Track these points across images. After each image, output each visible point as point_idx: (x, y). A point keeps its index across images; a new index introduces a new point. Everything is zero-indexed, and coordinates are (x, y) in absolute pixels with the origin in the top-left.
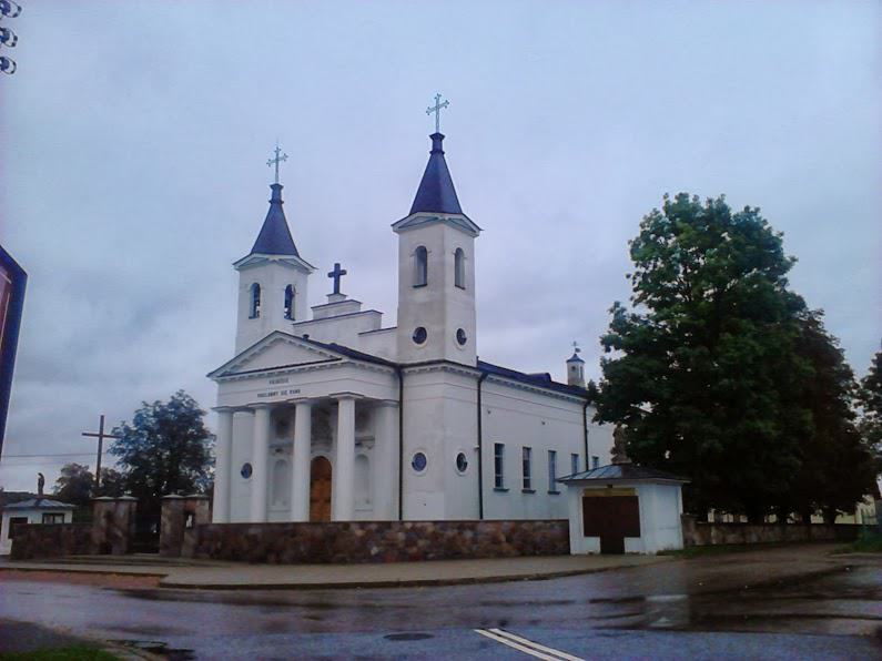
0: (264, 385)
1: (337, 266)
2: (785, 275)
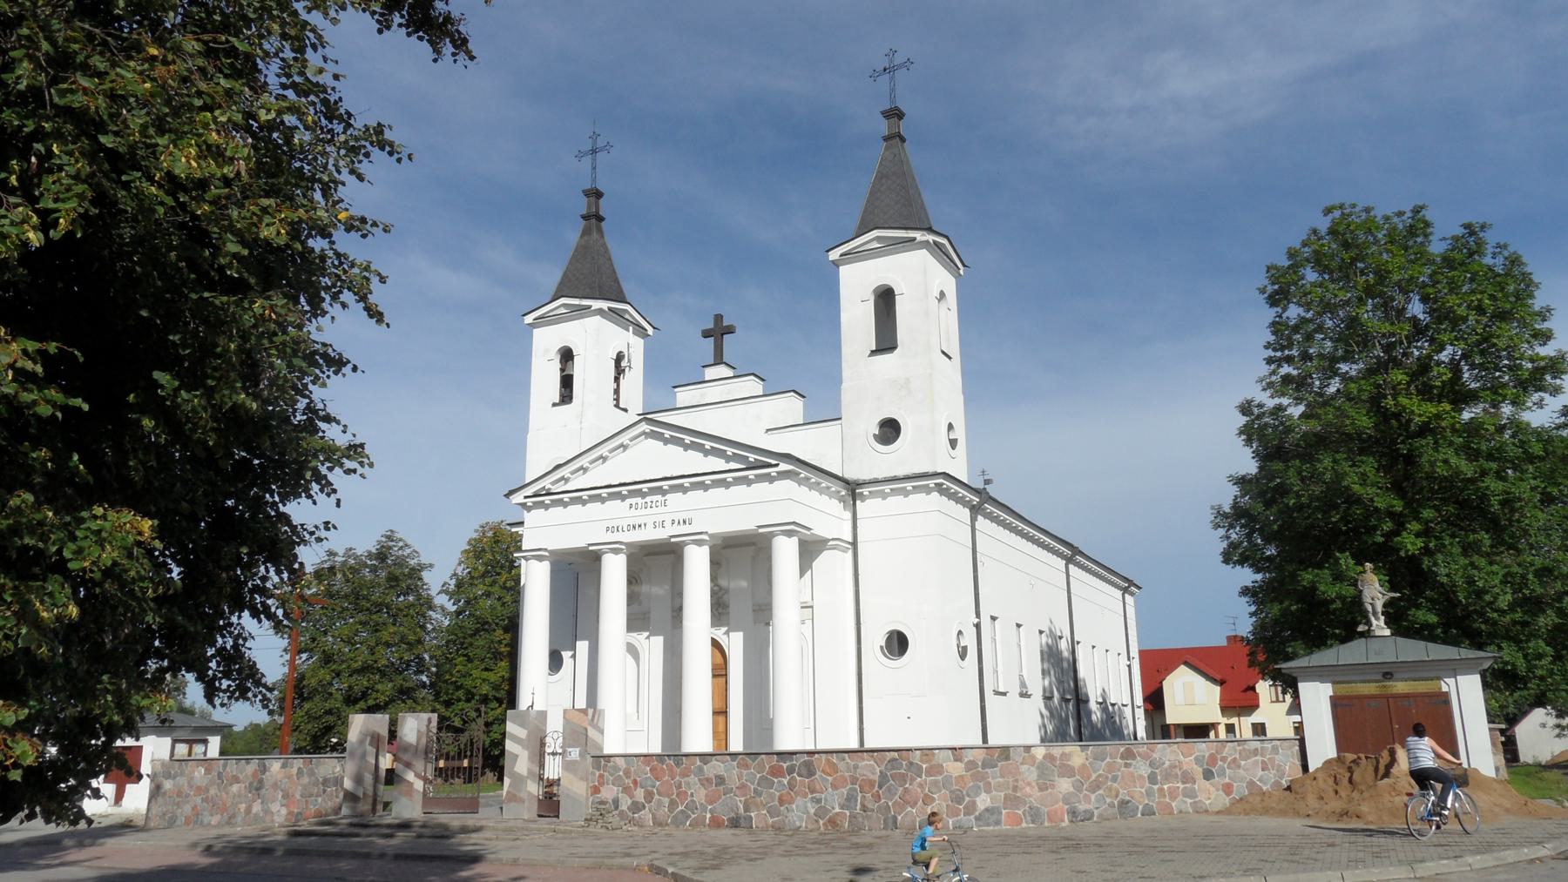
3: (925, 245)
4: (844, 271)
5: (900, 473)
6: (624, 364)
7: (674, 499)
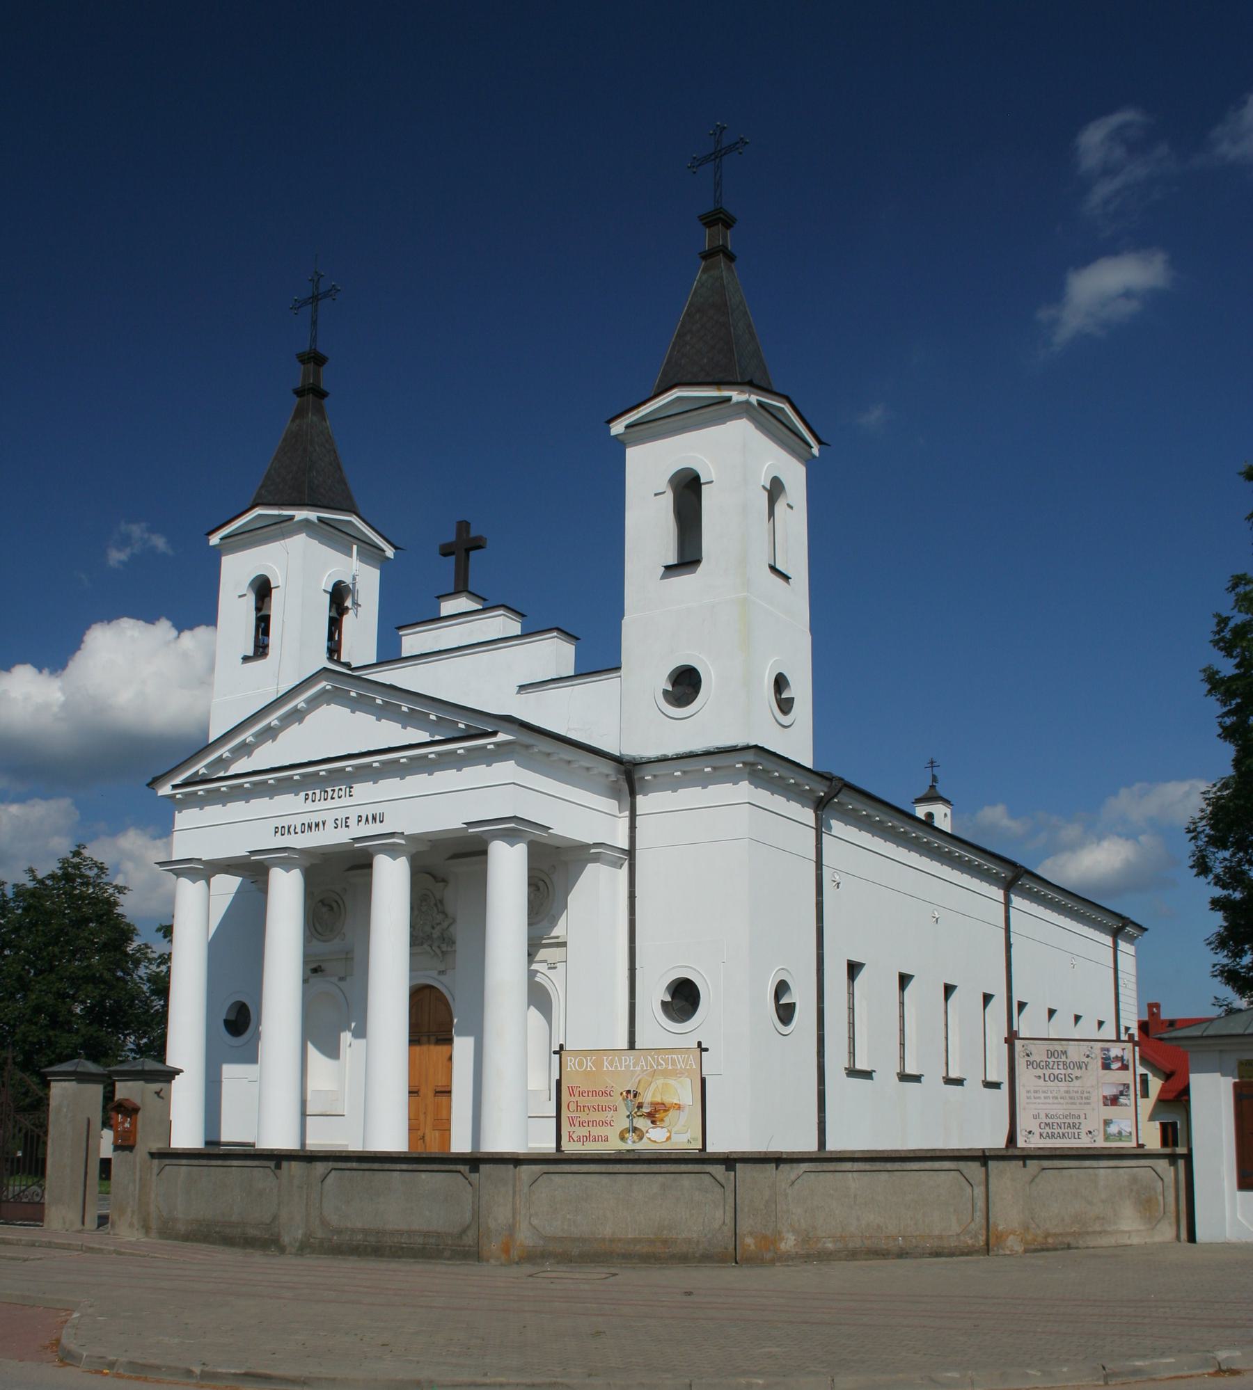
0: (290, 806)
1: (463, 526)
2: (1237, 671)
3: (745, 410)
4: (633, 455)
5: (698, 746)
6: (348, 603)
7: (364, 791)
